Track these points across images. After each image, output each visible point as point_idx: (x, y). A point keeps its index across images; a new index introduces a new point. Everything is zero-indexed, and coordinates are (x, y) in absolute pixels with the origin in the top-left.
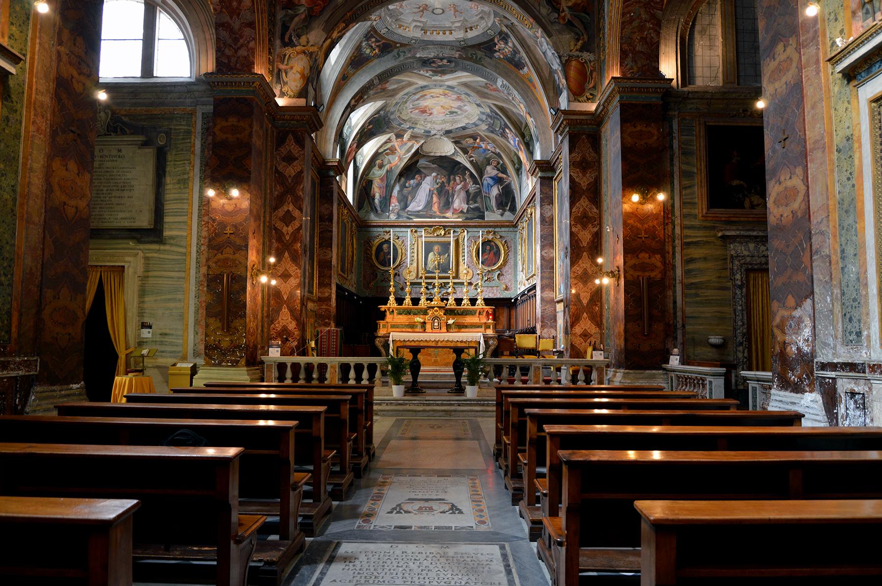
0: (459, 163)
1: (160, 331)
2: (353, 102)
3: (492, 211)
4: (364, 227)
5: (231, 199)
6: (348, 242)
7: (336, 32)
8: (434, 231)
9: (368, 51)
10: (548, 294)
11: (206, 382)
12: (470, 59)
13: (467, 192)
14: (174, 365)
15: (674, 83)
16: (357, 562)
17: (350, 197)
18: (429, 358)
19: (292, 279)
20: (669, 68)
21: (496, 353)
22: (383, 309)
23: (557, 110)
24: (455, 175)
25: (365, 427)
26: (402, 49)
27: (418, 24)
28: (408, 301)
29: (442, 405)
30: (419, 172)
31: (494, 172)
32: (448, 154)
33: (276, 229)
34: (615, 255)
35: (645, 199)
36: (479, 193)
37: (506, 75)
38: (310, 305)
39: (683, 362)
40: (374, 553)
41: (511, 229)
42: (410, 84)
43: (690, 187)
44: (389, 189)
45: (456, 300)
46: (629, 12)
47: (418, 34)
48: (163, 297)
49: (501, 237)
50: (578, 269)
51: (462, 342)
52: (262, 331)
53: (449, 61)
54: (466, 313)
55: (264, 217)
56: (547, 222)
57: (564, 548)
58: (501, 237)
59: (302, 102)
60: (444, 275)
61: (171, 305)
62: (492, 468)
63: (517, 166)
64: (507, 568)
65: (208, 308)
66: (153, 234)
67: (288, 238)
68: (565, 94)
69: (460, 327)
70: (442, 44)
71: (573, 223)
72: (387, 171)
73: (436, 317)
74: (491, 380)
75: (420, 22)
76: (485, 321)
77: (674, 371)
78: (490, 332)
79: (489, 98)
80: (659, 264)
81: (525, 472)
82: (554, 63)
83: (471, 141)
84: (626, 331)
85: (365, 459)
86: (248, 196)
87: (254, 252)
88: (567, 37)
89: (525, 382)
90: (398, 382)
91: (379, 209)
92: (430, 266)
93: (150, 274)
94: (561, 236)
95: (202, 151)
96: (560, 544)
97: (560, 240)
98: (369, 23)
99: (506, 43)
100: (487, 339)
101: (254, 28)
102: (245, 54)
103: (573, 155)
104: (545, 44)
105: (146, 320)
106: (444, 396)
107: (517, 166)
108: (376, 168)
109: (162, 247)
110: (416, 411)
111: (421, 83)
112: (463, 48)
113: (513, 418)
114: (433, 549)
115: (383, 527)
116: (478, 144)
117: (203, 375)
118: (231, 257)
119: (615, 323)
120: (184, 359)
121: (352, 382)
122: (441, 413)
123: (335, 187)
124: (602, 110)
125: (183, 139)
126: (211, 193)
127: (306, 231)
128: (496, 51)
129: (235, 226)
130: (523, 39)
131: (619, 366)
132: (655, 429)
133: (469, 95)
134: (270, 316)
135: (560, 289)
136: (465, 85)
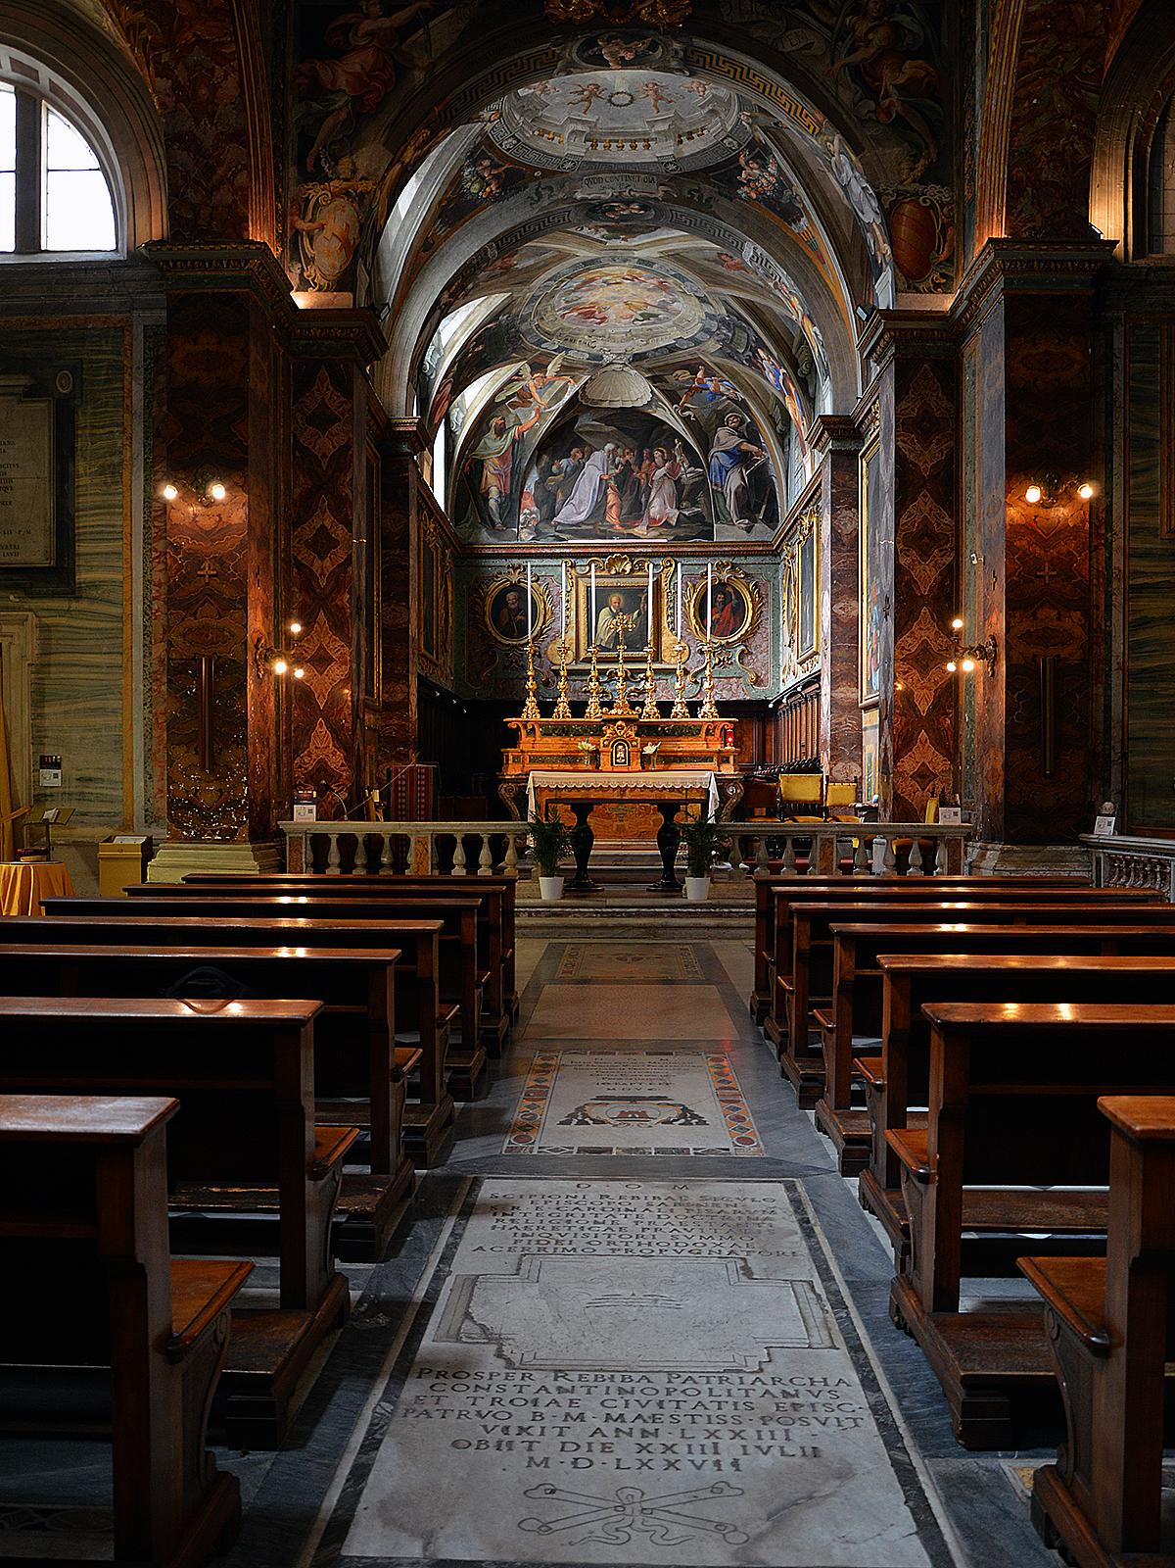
1: (76, 774)
2: (445, 298)
3: (729, 519)
4: (468, 560)
5: (210, 503)
6: (437, 590)
7: (411, 149)
8: (610, 565)
11: (187, 873)
12: (687, 202)
13: (678, 482)
14: (110, 840)
15: (1119, 247)
16: (517, 1215)
18: (607, 822)
20: (1108, 218)
21: (741, 812)
23: (872, 310)
24: (652, 449)
25: (503, 959)
26: (545, 182)
27: (579, 127)
28: (562, 707)
29: (639, 915)
30: (578, 442)
32: (639, 404)
33: (299, 565)
34: (988, 612)
35: (1052, 496)
36: (701, 485)
37: (762, 236)
38: (369, 718)
39: (1120, 829)
40: (547, 1198)
42: (562, 257)
43: (1146, 470)
44: (518, 478)
45: (659, 705)
46: (1029, 97)
47: (579, 149)
48: (80, 706)
49: (747, 575)
50: (912, 643)
51: (672, 789)
52: (278, 770)
54: (679, 731)
55: (275, 540)
56: (845, 545)
57: (933, 1190)
58: (747, 575)
59: (344, 300)
60: (636, 654)
61: (99, 721)
62: (750, 1039)
64: (804, 1222)
65: (172, 725)
66: (56, 578)
67: (323, 583)
68: (887, 275)
69: (668, 760)
70: (629, 170)
71: (901, 547)
72: (514, 441)
73: (621, 741)
74: (735, 865)
75: (583, 122)
76: (718, 747)
77: (1104, 846)
78: (728, 770)
79: (724, 285)
80: (1078, 631)
81: (827, 1046)
82: (867, 208)
84: (1007, 766)
85: (505, 1021)
86: (243, 497)
87: (259, 612)
88: (894, 152)
89: (802, 869)
90: (550, 872)
91: (497, 520)
93: (53, 658)
94: (874, 572)
95: (147, 407)
96: (925, 1179)
97: (870, 581)
98: (478, 126)
99: (764, 167)
100: (722, 784)
101: (245, 144)
102: (229, 199)
103: (903, 404)
104: (847, 167)
105: (50, 751)
106: (641, 898)
108: (492, 434)
109: (74, 605)
110: (587, 928)
112: (673, 178)
113: (801, 940)
114: (658, 1190)
115: (556, 1150)
117: (167, 860)
118: (214, 623)
119: (986, 751)
120: (127, 828)
121: (458, 871)
122: (637, 932)
123: (412, 475)
124: (966, 310)
125: (108, 381)
126: (170, 493)
127: (359, 568)
128: (742, 184)
129: (220, 561)
130: (800, 157)
131: (990, 837)
132: (1062, 962)
133: (683, 279)
134: (294, 740)
135: (870, 682)
136: (676, 257)
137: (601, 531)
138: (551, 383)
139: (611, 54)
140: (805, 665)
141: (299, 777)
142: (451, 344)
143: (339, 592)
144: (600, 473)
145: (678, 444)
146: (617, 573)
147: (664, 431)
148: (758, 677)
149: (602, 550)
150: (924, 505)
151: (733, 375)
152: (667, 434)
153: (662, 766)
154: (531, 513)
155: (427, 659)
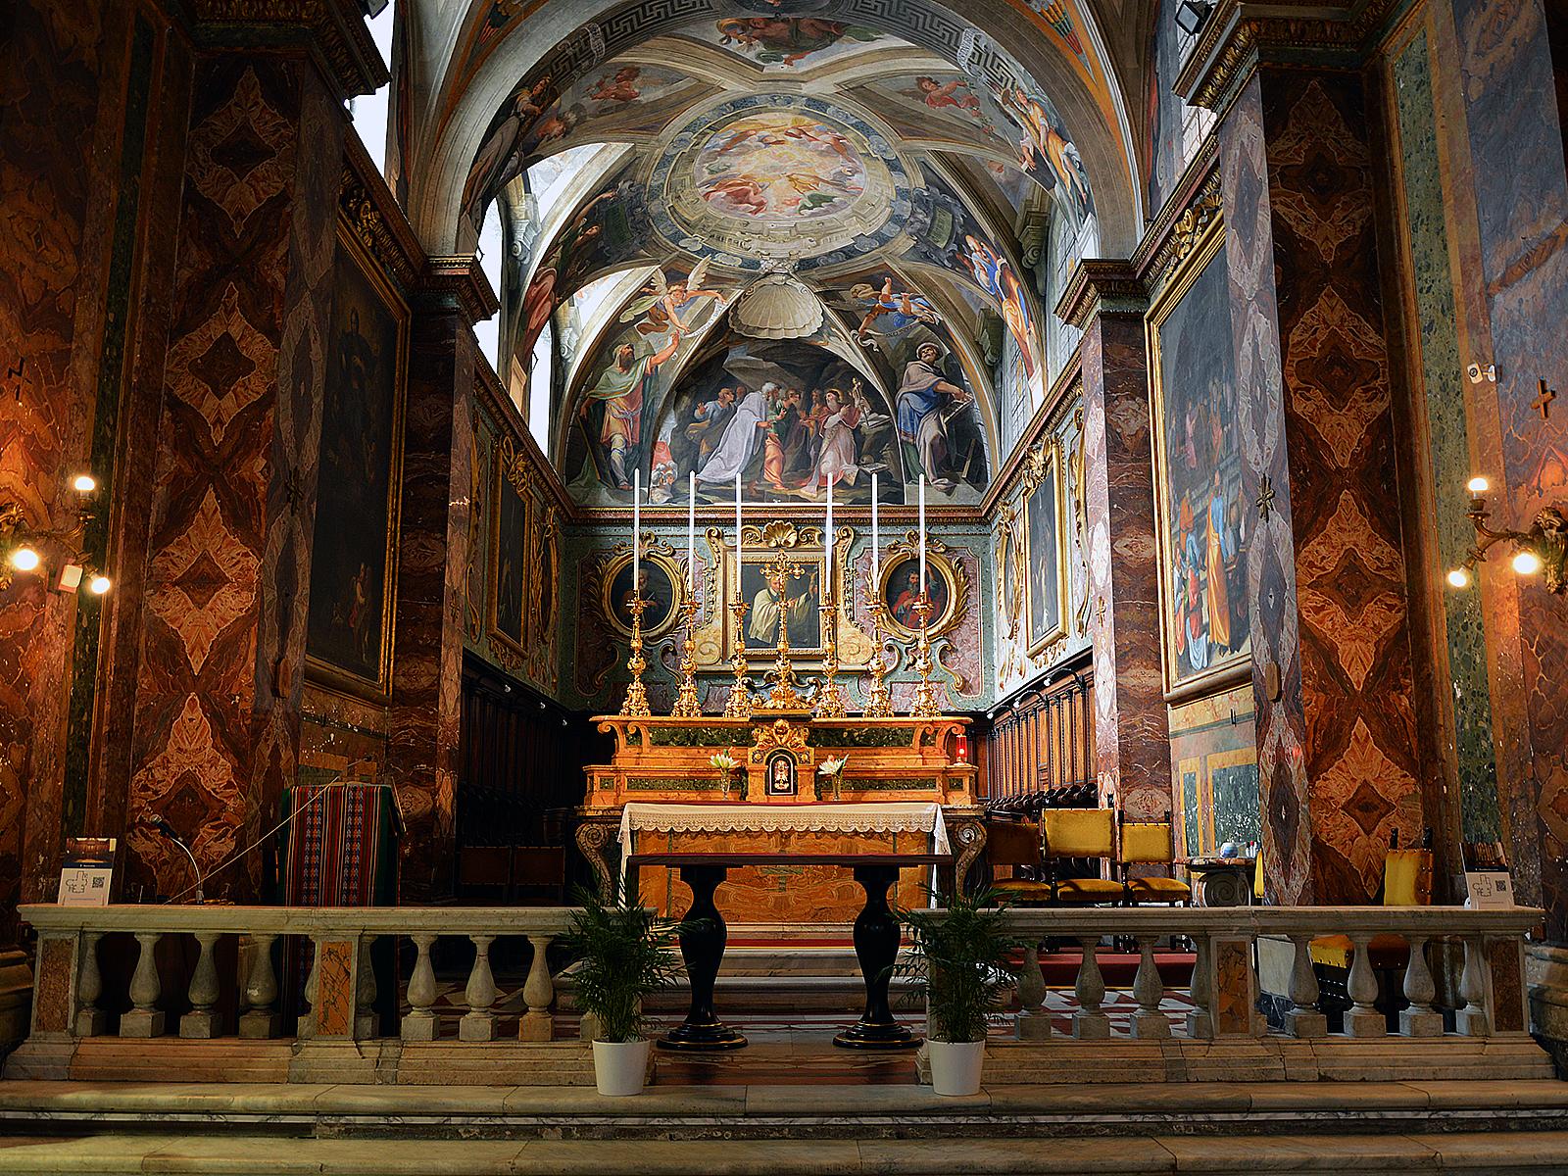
0: (836, 358)
4: (582, 529)
8: (769, 536)
10: (1142, 678)
13: (857, 431)
17: (539, 428)
19: (226, 592)
22: (604, 728)
30: (729, 381)
32: (806, 333)
33: (175, 404)
36: (886, 435)
41: (974, 529)
42: (703, 89)
44: (649, 425)
49: (948, 549)
50: (1326, 553)
58: (948, 549)
63: (989, 356)
67: (217, 437)
69: (862, 785)
71: (1293, 383)
72: (645, 376)
73: (783, 754)
76: (942, 764)
78: (962, 801)
79: (923, 135)
92: (760, 627)
100: (954, 823)
107: (989, 356)
108: (616, 367)
111: (734, 87)
136: (859, 91)
137: (758, 492)
138: (693, 300)
140: (1041, 657)
141: (141, 809)
143: (247, 453)
144: (758, 419)
146: (778, 546)
147: (838, 369)
148: (965, 681)
149: (758, 516)
150: (1329, 312)
151: (929, 288)
152: (842, 372)
153: (850, 796)
154: (667, 469)
155: (512, 649)
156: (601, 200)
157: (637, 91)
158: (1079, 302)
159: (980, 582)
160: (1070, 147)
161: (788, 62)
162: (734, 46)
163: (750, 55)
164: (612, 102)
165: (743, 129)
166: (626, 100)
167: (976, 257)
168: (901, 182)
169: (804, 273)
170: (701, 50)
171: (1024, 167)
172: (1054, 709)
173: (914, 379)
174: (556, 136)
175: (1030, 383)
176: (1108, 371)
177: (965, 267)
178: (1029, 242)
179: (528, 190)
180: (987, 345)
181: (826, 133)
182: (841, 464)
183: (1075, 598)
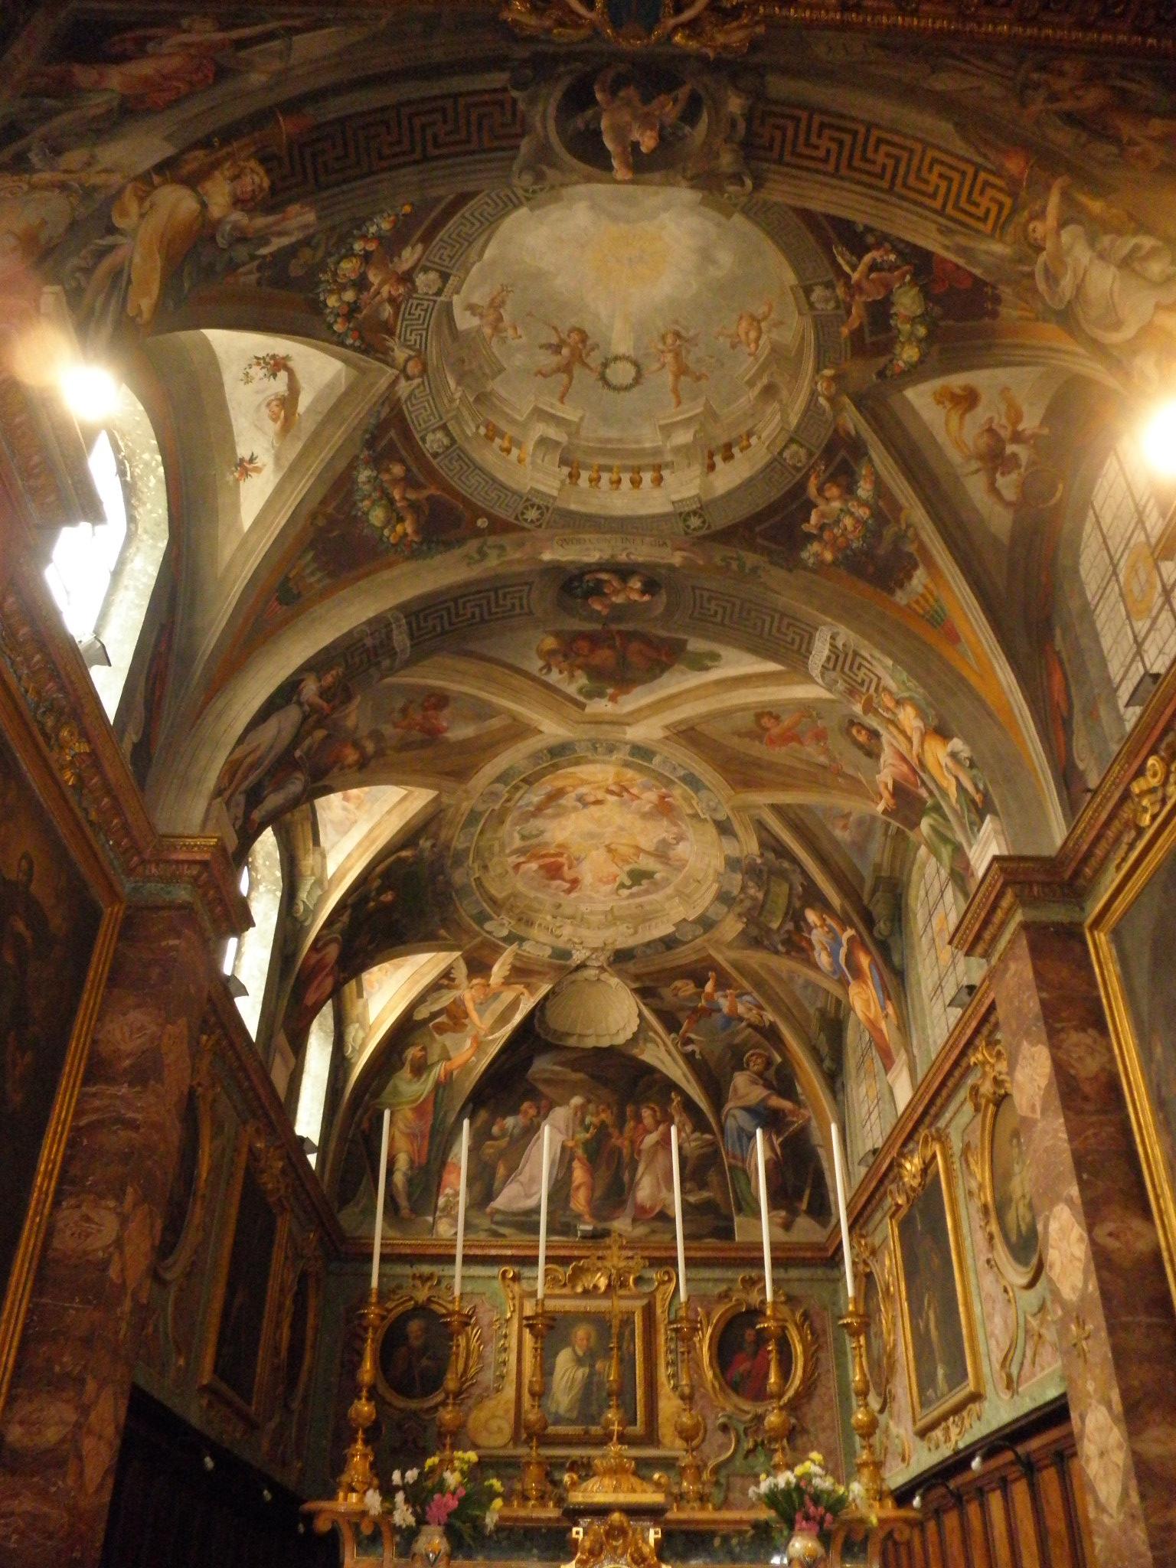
0: (650, 1070)
8: (574, 1278)
9: (377, 516)
17: (308, 1122)
22: (322, 1525)
24: (638, 1104)
31: (756, 1094)
32: (620, 1040)
41: (820, 1272)
42: (519, 730)
44: (440, 1141)
53: (651, 587)
63: (827, 1063)
72: (438, 1085)
75: (559, 421)
83: (687, 988)
99: (849, 490)
107: (827, 1063)
108: (406, 1073)
111: (552, 729)
116: (710, 998)
136: (689, 735)
138: (496, 995)
139: (620, 132)
140: (938, 1433)
142: (379, 1020)
145: (676, 1099)
156: (399, 859)
157: (445, 724)
158: (986, 922)
159: (830, 1339)
160: (957, 744)
161: (613, 699)
162: (554, 677)
163: (571, 689)
164: (416, 735)
165: (559, 784)
166: (432, 736)
167: (817, 936)
168: (731, 848)
169: (619, 966)
170: (517, 681)
171: (880, 808)
172: (973, 1509)
173: (742, 1091)
174: (350, 767)
175: (890, 1077)
176: (1044, 995)
177: (801, 950)
178: (880, 910)
179: (316, 841)
180: (825, 1050)
181: (650, 789)
182: (660, 1191)
183: (993, 1343)
